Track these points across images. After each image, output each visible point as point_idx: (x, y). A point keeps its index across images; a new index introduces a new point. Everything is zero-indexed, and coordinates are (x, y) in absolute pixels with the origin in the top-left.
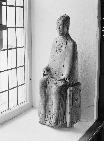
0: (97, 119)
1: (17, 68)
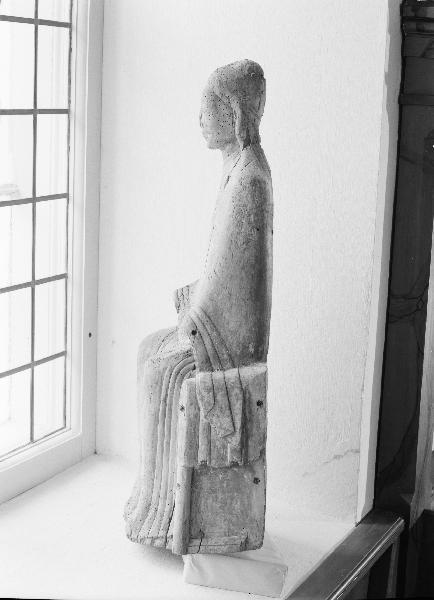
1: (33, 284)
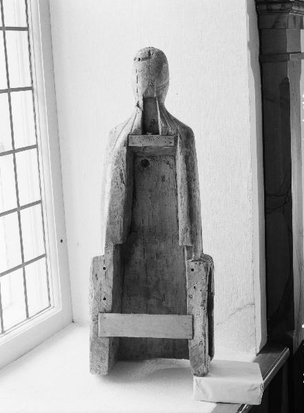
0: (264, 345)
